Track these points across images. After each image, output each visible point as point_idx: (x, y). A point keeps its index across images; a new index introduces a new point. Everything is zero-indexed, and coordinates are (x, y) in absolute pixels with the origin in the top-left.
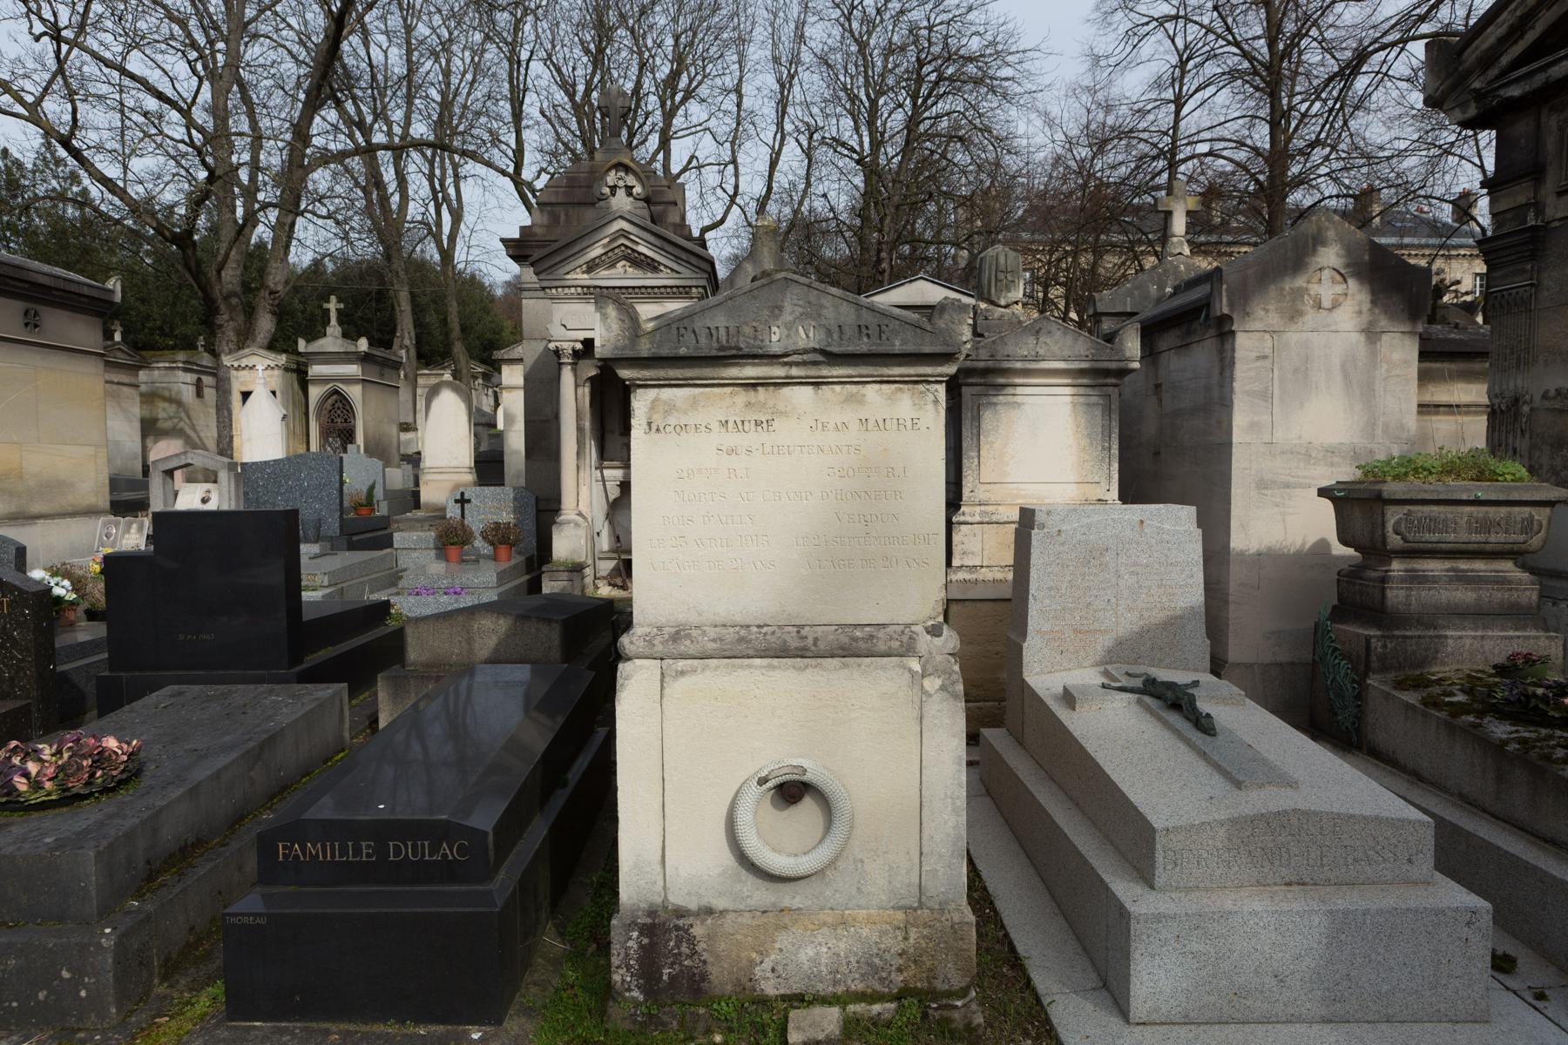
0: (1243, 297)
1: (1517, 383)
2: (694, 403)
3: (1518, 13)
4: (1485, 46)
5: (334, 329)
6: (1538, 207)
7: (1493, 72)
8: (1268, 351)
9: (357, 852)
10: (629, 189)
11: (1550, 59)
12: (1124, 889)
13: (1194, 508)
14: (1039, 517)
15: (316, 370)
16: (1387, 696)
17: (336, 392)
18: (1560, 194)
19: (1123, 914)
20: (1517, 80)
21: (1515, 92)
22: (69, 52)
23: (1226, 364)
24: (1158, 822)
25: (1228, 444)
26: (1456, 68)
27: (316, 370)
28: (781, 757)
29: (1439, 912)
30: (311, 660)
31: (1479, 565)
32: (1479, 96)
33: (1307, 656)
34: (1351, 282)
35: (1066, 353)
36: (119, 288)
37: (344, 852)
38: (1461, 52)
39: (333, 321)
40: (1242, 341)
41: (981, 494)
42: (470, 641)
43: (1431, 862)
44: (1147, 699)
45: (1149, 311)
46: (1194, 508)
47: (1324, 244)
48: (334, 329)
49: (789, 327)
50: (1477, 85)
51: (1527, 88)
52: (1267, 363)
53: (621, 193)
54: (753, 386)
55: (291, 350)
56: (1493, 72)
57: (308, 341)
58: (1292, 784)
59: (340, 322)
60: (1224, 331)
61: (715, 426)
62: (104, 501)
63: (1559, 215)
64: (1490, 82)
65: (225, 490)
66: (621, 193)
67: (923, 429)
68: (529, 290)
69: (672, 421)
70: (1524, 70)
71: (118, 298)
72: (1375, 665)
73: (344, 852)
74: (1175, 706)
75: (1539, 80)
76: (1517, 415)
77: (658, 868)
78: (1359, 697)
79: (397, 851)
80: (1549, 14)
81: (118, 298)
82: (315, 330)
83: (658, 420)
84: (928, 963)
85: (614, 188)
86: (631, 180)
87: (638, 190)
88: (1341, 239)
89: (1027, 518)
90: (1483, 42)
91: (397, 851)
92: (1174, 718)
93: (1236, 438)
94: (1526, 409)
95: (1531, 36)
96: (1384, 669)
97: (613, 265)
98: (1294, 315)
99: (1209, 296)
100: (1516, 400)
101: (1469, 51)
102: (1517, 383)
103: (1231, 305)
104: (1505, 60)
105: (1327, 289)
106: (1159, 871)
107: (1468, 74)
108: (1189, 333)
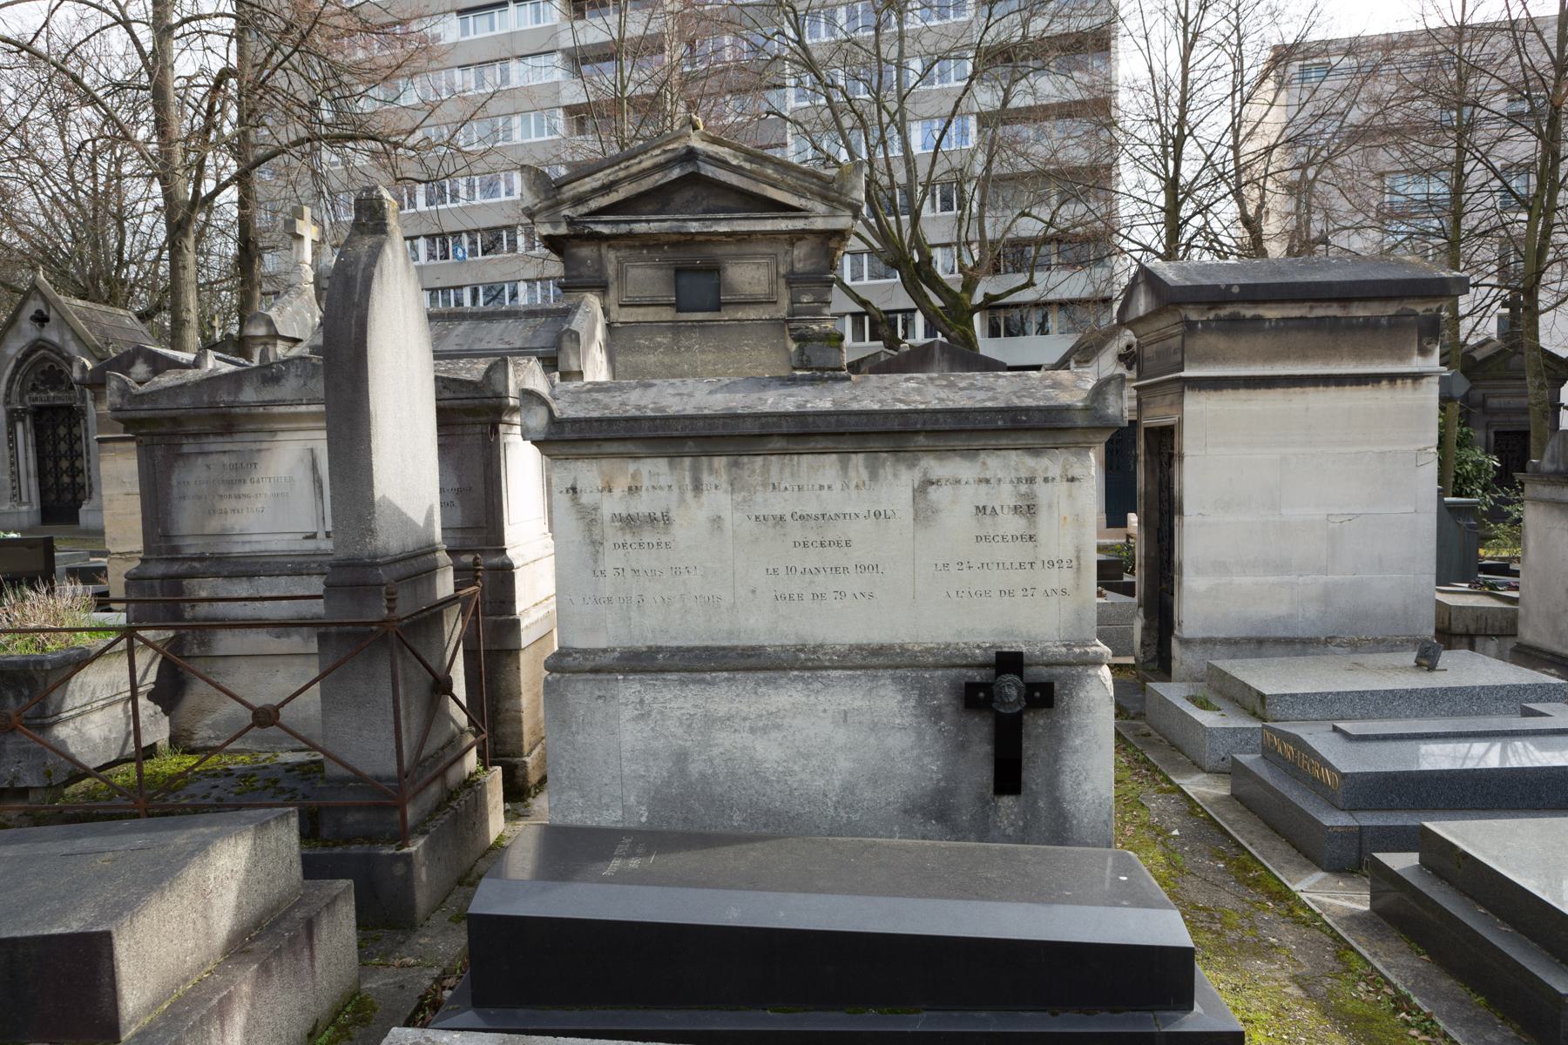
3: (611, 178)
4: (582, 189)
7: (583, 209)
11: (634, 218)
20: (606, 223)
21: (605, 230)
22: (291, 63)
26: (554, 196)
31: (402, 713)
45: (848, 383)
51: (614, 231)
56: (583, 209)
63: (621, 320)
64: (581, 216)
67: (610, 572)
68: (283, 626)
75: (624, 228)
80: (630, 187)
84: (796, 768)
90: (581, 185)
95: (614, 197)
101: (569, 187)
104: (594, 204)
107: (560, 203)
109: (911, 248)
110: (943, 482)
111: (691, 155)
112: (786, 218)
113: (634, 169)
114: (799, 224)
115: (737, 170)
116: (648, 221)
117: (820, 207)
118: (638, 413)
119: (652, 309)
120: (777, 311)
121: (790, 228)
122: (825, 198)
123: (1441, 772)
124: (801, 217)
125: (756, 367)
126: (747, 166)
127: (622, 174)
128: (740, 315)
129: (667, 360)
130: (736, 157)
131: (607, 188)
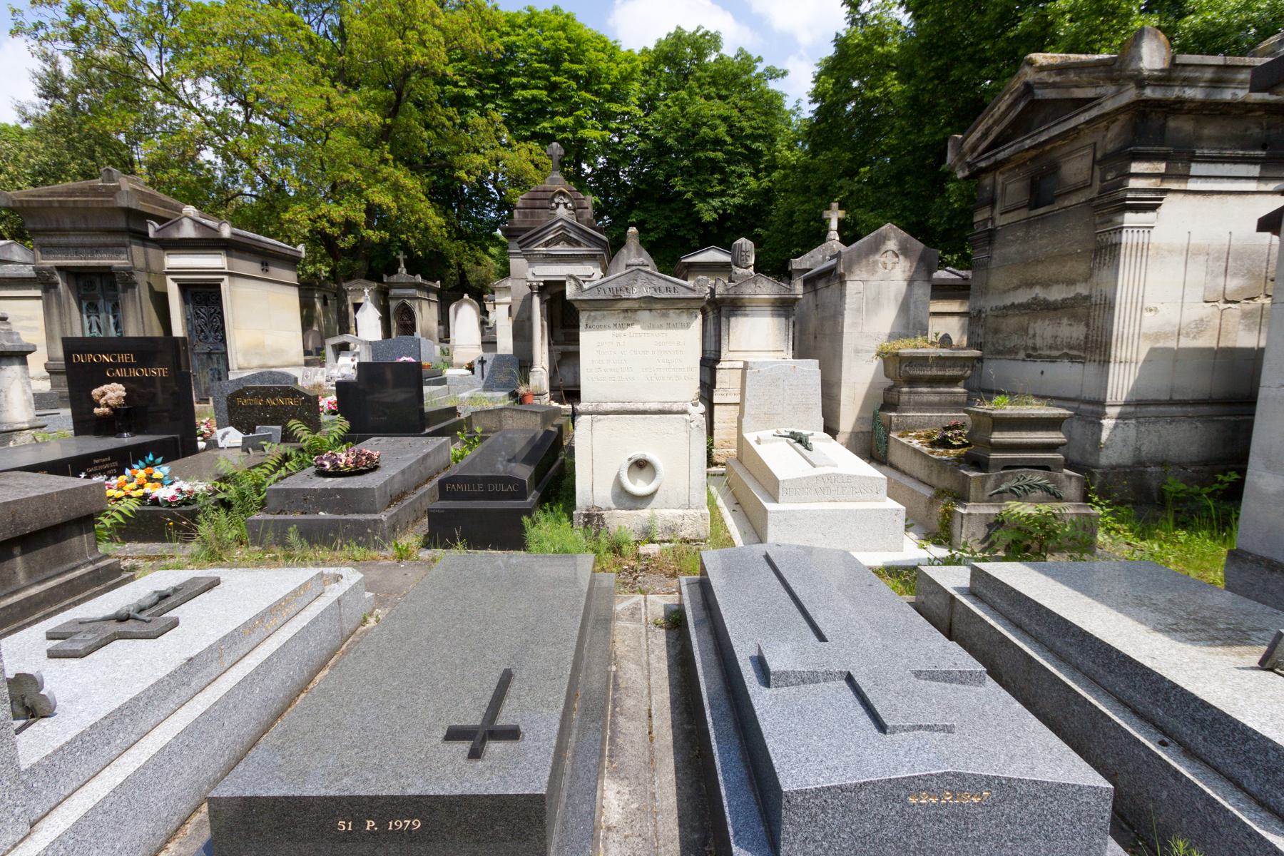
0: (849, 268)
1: (981, 303)
2: (604, 317)
5: (402, 270)
6: (992, 219)
7: (975, 154)
8: (861, 290)
9: (476, 488)
10: (565, 205)
12: (770, 506)
13: (817, 361)
14: (750, 365)
15: (393, 292)
16: (896, 440)
17: (404, 304)
18: (1001, 214)
19: (766, 511)
21: (983, 164)
23: (842, 296)
24: (780, 478)
25: (842, 332)
27: (393, 292)
28: (638, 454)
29: (884, 510)
30: (427, 431)
32: (969, 165)
33: (866, 428)
34: (901, 257)
35: (769, 292)
36: (303, 251)
37: (471, 488)
38: (962, 144)
39: (402, 265)
40: (850, 286)
41: (731, 355)
42: (500, 421)
43: (885, 493)
44: (790, 440)
46: (817, 361)
47: (889, 240)
48: (402, 270)
49: (640, 287)
50: (968, 160)
52: (861, 295)
53: (562, 207)
54: (626, 311)
55: (380, 280)
57: (388, 276)
58: (836, 466)
59: (406, 266)
60: (842, 281)
61: (612, 326)
62: (303, 362)
65: (235, 362)
66: (562, 207)
69: (596, 324)
70: (987, 155)
71: (303, 255)
72: (893, 428)
73: (471, 488)
74: (800, 441)
75: (993, 159)
76: (980, 318)
77: (590, 493)
78: (886, 442)
79: (491, 488)
81: (303, 255)
82: (393, 270)
83: (590, 323)
85: (558, 204)
86: (566, 201)
87: (570, 205)
88: (896, 237)
89: (746, 366)
91: (491, 488)
92: (798, 446)
93: (845, 330)
94: (983, 315)
95: (991, 138)
96: (897, 430)
97: (558, 244)
98: (874, 272)
99: (836, 264)
100: (980, 311)
102: (981, 303)
103: (844, 268)
104: (980, 149)
105: (889, 259)
106: (780, 496)
108: (829, 281)
109: (115, 358)
110: (445, 346)
111: (1029, 88)
112: (1083, 112)
113: (996, 115)
114: (1094, 113)
115: (1054, 85)
116: (1004, 150)
117: (1111, 89)
118: (593, 314)
119: (1016, 212)
120: (1091, 193)
121: (1087, 118)
122: (1114, 81)
123: (770, 760)
124: (1095, 106)
125: (1072, 245)
126: (1058, 79)
127: (991, 122)
128: (1066, 203)
129: (1021, 249)
130: (1050, 76)
131: (985, 135)
